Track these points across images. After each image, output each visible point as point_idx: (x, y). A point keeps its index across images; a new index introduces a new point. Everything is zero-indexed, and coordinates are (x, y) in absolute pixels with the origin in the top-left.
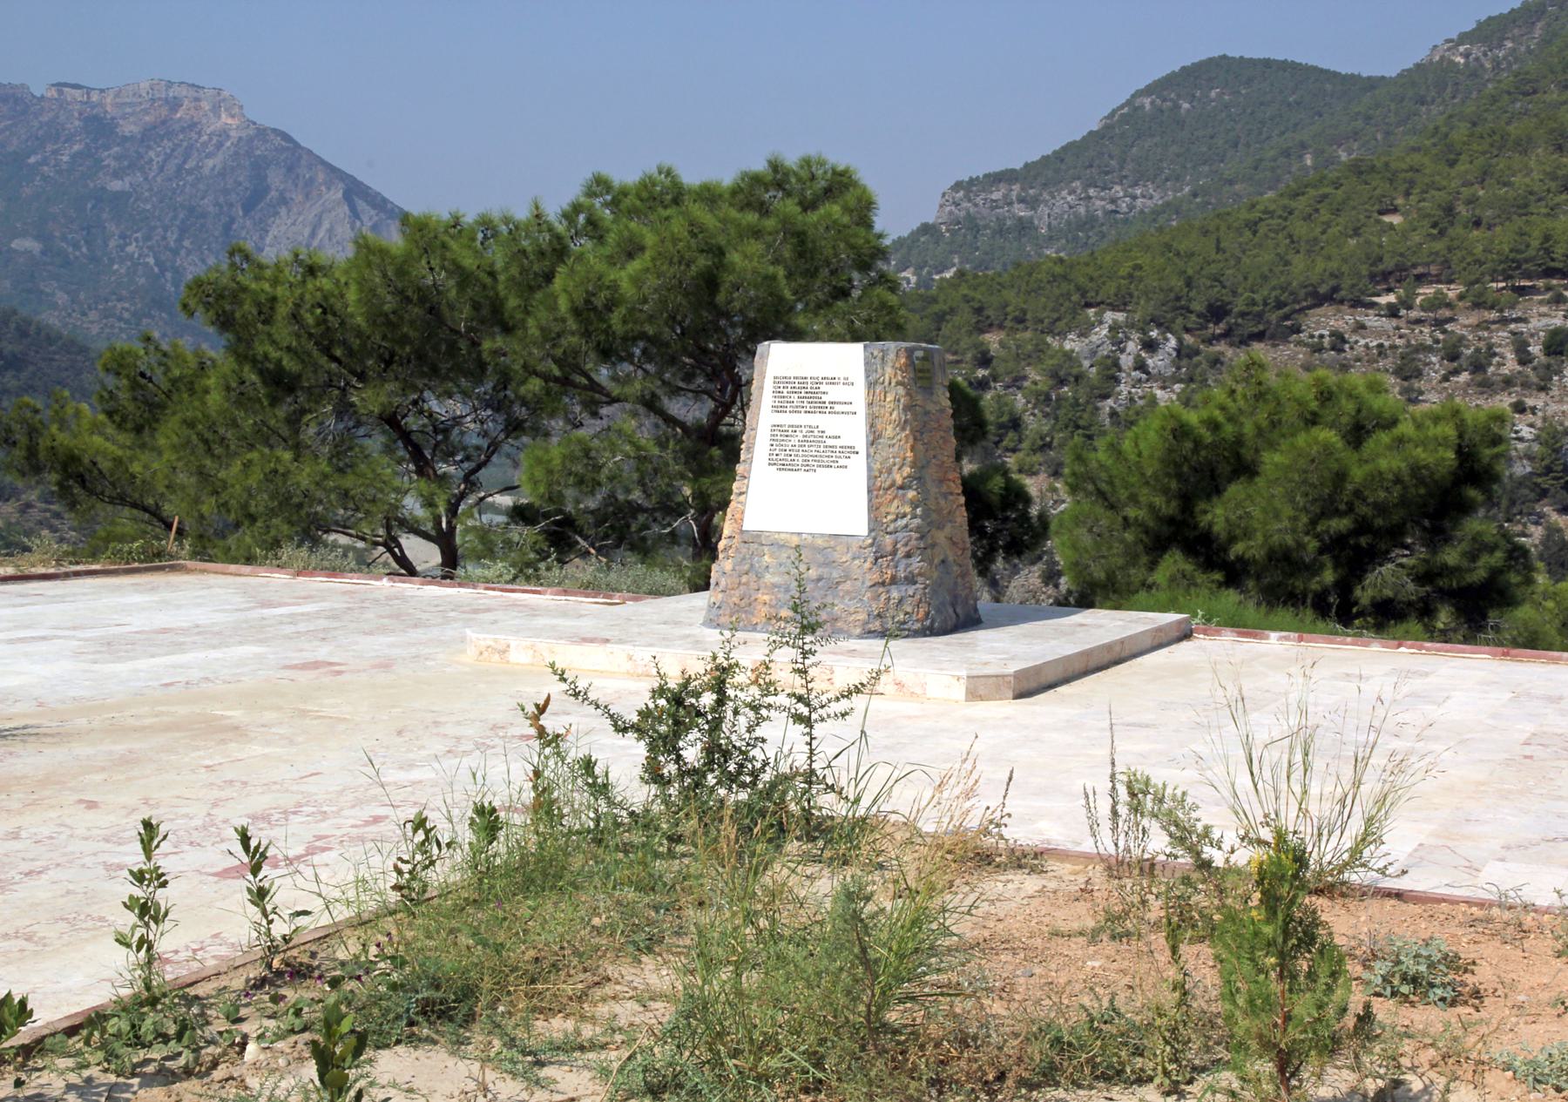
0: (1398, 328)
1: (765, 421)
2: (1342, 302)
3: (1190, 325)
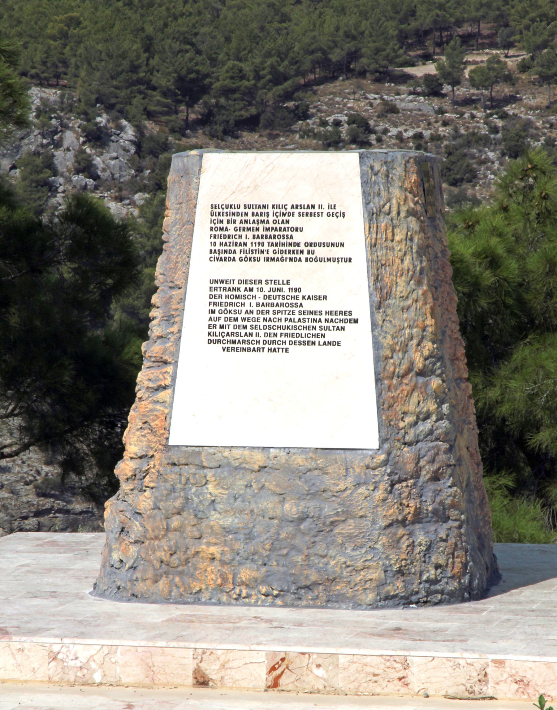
0: (441, 111)
1: (197, 276)
2: (362, 74)
3: (152, 108)
